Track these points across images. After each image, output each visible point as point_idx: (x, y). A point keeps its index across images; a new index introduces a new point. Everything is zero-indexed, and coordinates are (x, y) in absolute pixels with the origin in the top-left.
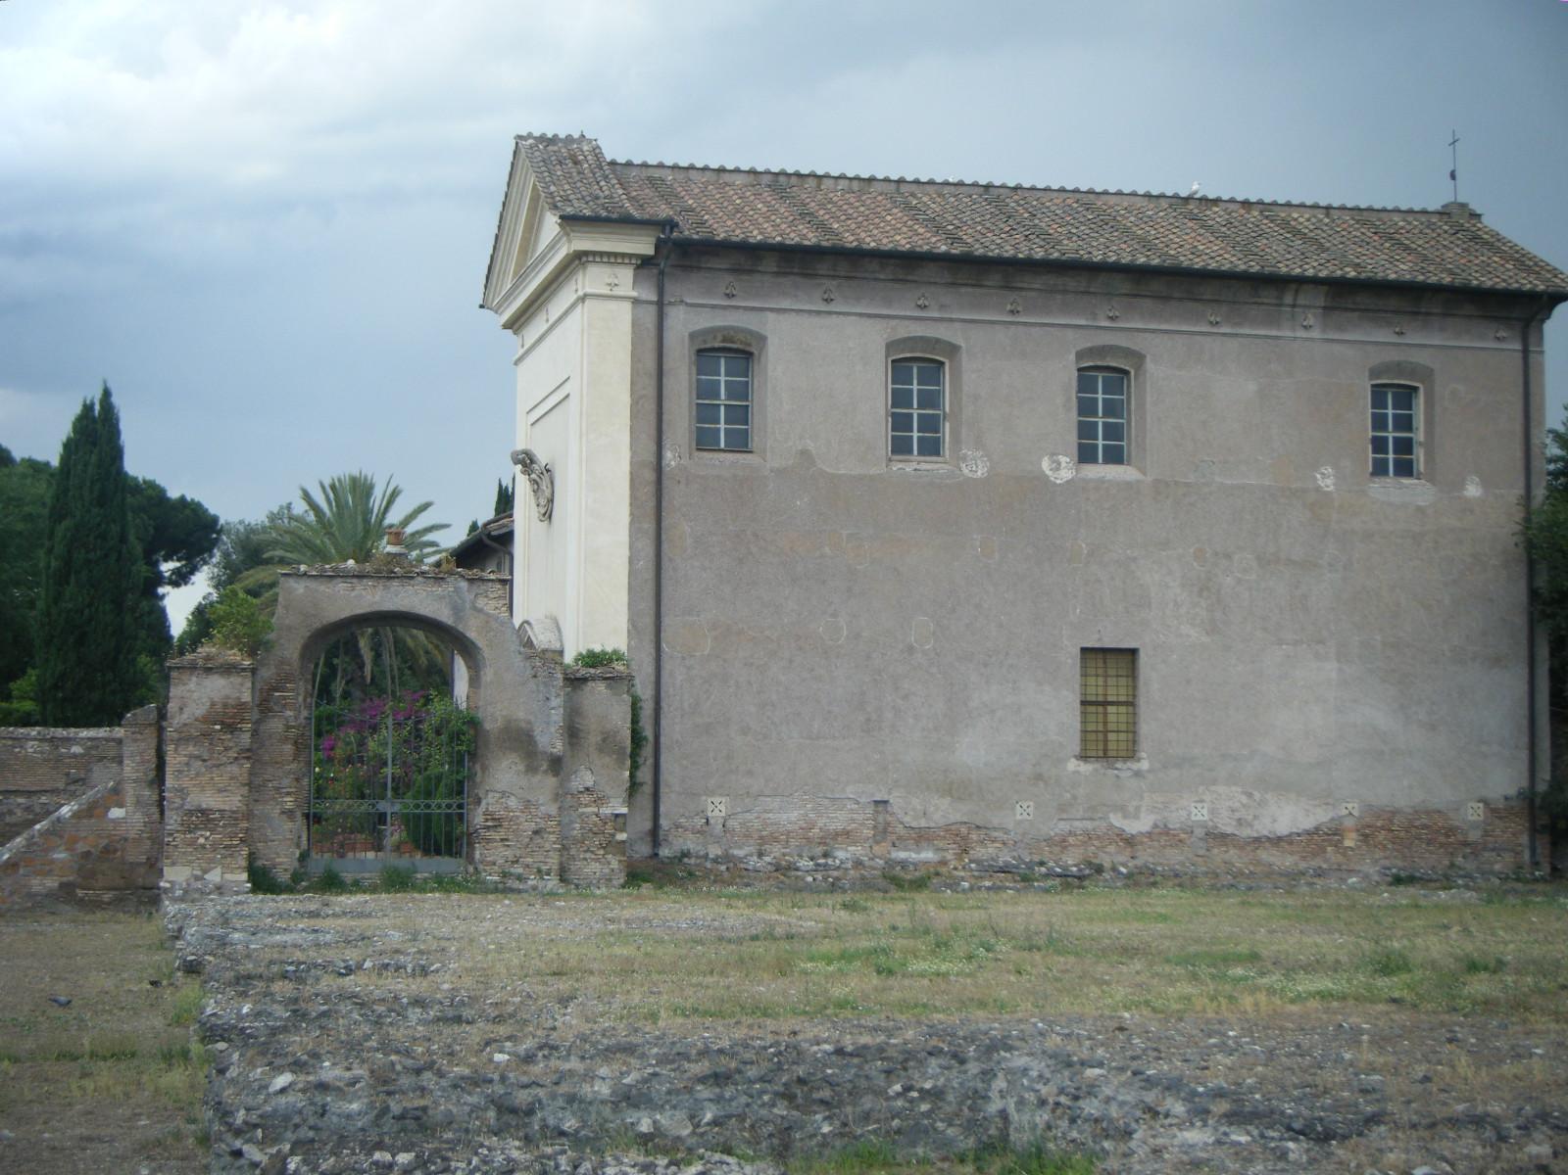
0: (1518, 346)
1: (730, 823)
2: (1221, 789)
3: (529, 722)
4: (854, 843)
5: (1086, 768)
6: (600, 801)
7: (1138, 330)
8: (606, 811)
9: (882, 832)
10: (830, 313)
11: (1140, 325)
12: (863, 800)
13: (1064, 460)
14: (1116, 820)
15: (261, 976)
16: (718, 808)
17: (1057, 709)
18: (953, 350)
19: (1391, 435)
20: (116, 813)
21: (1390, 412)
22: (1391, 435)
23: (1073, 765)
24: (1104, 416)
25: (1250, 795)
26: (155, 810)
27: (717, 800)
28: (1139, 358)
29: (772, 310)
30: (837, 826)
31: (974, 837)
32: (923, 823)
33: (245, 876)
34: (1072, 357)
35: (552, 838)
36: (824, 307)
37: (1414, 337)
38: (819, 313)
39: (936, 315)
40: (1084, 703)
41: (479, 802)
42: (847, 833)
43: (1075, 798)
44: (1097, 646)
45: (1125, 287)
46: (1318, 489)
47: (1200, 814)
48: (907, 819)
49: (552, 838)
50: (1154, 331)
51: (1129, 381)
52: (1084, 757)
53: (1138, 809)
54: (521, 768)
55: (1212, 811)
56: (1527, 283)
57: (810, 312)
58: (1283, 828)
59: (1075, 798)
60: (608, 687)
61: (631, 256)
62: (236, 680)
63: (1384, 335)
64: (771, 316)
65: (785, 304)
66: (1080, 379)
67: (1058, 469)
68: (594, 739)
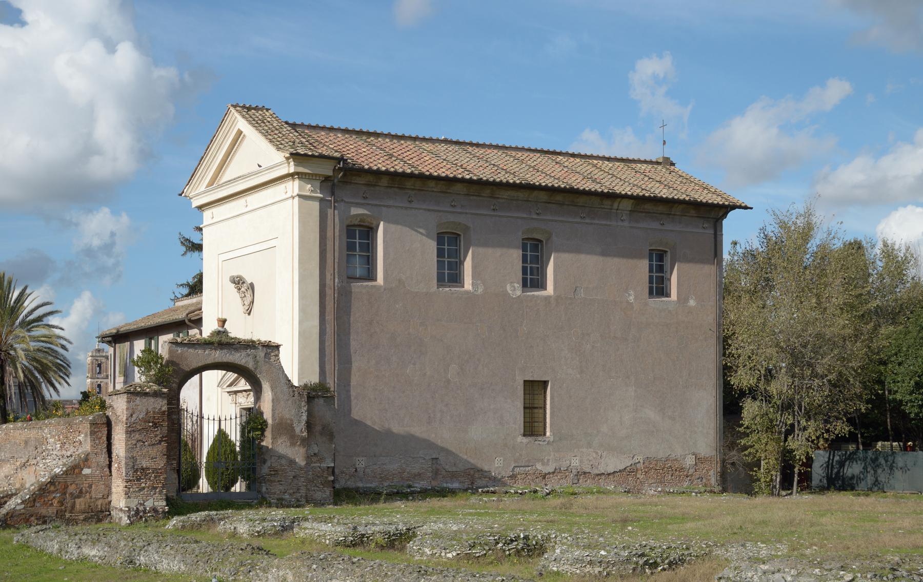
0: (712, 232)
1: (367, 470)
2: (584, 450)
3: (291, 420)
4: (423, 480)
5: (525, 440)
6: (321, 460)
7: (550, 220)
8: (324, 465)
9: (436, 473)
10: (411, 208)
11: (550, 218)
12: (427, 458)
13: (516, 285)
14: (539, 466)
15: (773, 573)
16: (361, 463)
17: (513, 411)
18: (466, 229)
19: (655, 275)
20: (86, 471)
21: (529, 253)
22: (655, 275)
23: (520, 439)
24: (448, 257)
25: (597, 453)
26: (107, 469)
27: (360, 459)
28: (466, 229)
29: (384, 206)
30: (416, 471)
31: (477, 476)
32: (454, 469)
33: (164, 503)
34: (520, 233)
35: (303, 479)
36: (408, 205)
37: (669, 227)
38: (406, 208)
39: (460, 210)
40: (525, 408)
41: (264, 462)
42: (419, 474)
43: (521, 455)
44: (531, 379)
45: (693, 212)
46: (628, 302)
47: (575, 463)
48: (447, 467)
49: (303, 479)
50: (556, 221)
51: (542, 245)
52: (524, 435)
53: (548, 460)
54: (288, 444)
55: (581, 461)
56: (718, 200)
57: (402, 207)
58: (611, 469)
59: (521, 455)
60: (325, 401)
61: (320, 175)
62: (159, 400)
63: (655, 225)
64: (384, 209)
65: (391, 203)
66: (348, 230)
67: (515, 290)
68: (318, 428)
